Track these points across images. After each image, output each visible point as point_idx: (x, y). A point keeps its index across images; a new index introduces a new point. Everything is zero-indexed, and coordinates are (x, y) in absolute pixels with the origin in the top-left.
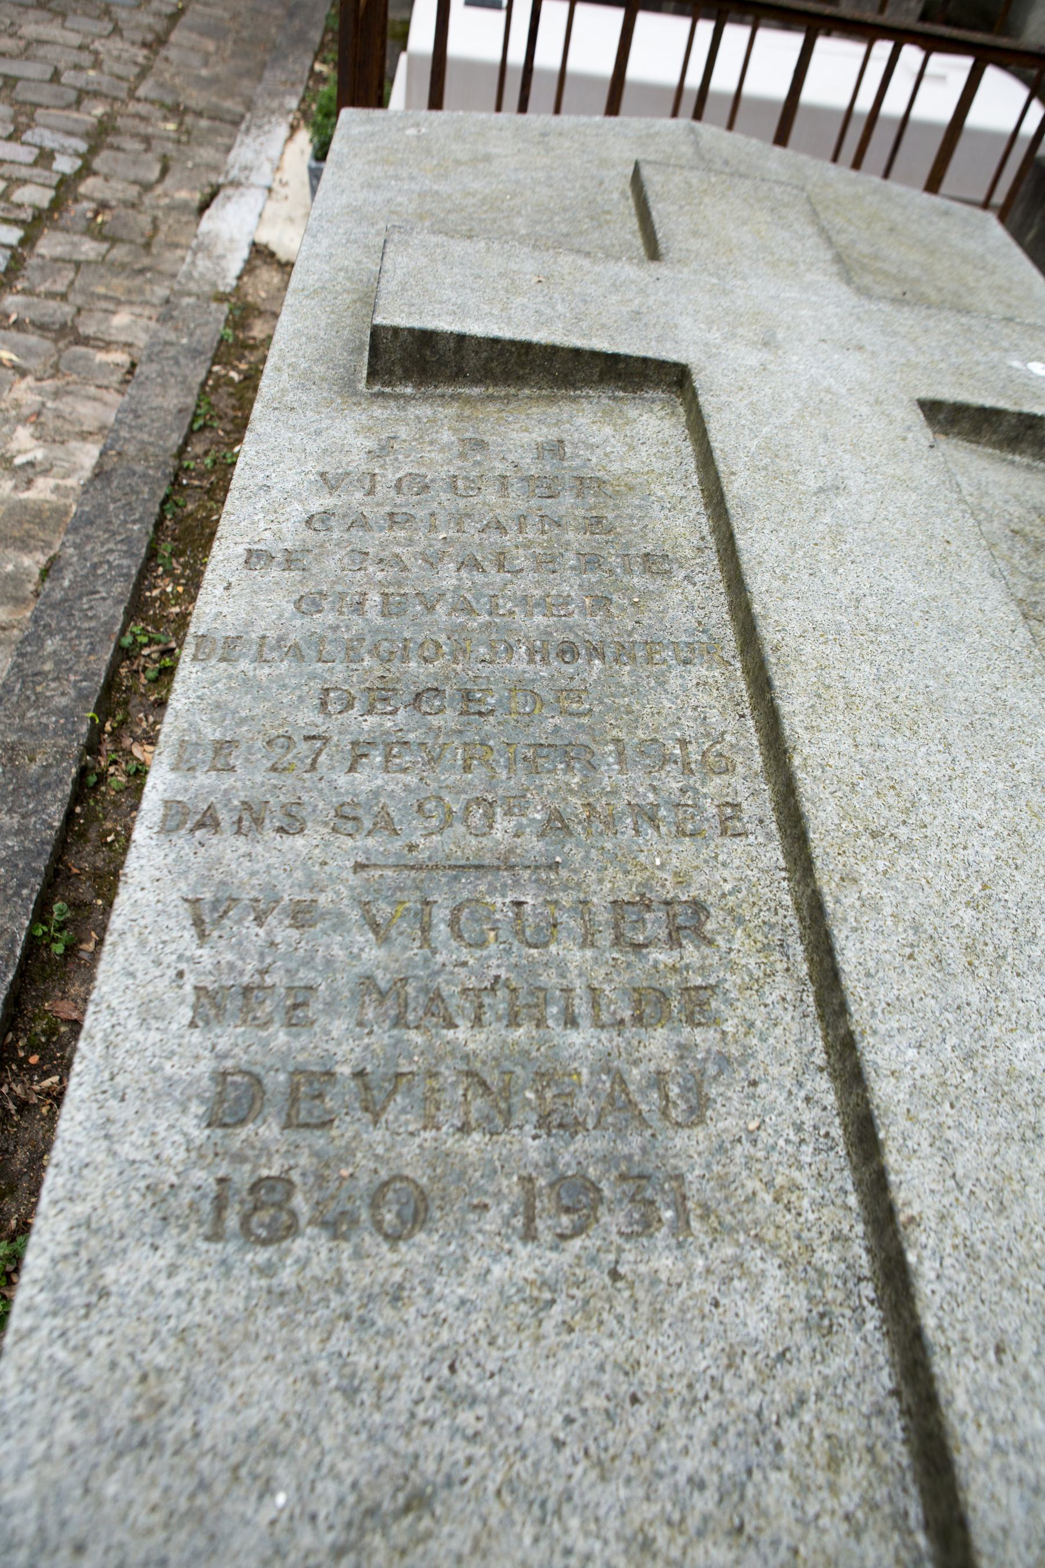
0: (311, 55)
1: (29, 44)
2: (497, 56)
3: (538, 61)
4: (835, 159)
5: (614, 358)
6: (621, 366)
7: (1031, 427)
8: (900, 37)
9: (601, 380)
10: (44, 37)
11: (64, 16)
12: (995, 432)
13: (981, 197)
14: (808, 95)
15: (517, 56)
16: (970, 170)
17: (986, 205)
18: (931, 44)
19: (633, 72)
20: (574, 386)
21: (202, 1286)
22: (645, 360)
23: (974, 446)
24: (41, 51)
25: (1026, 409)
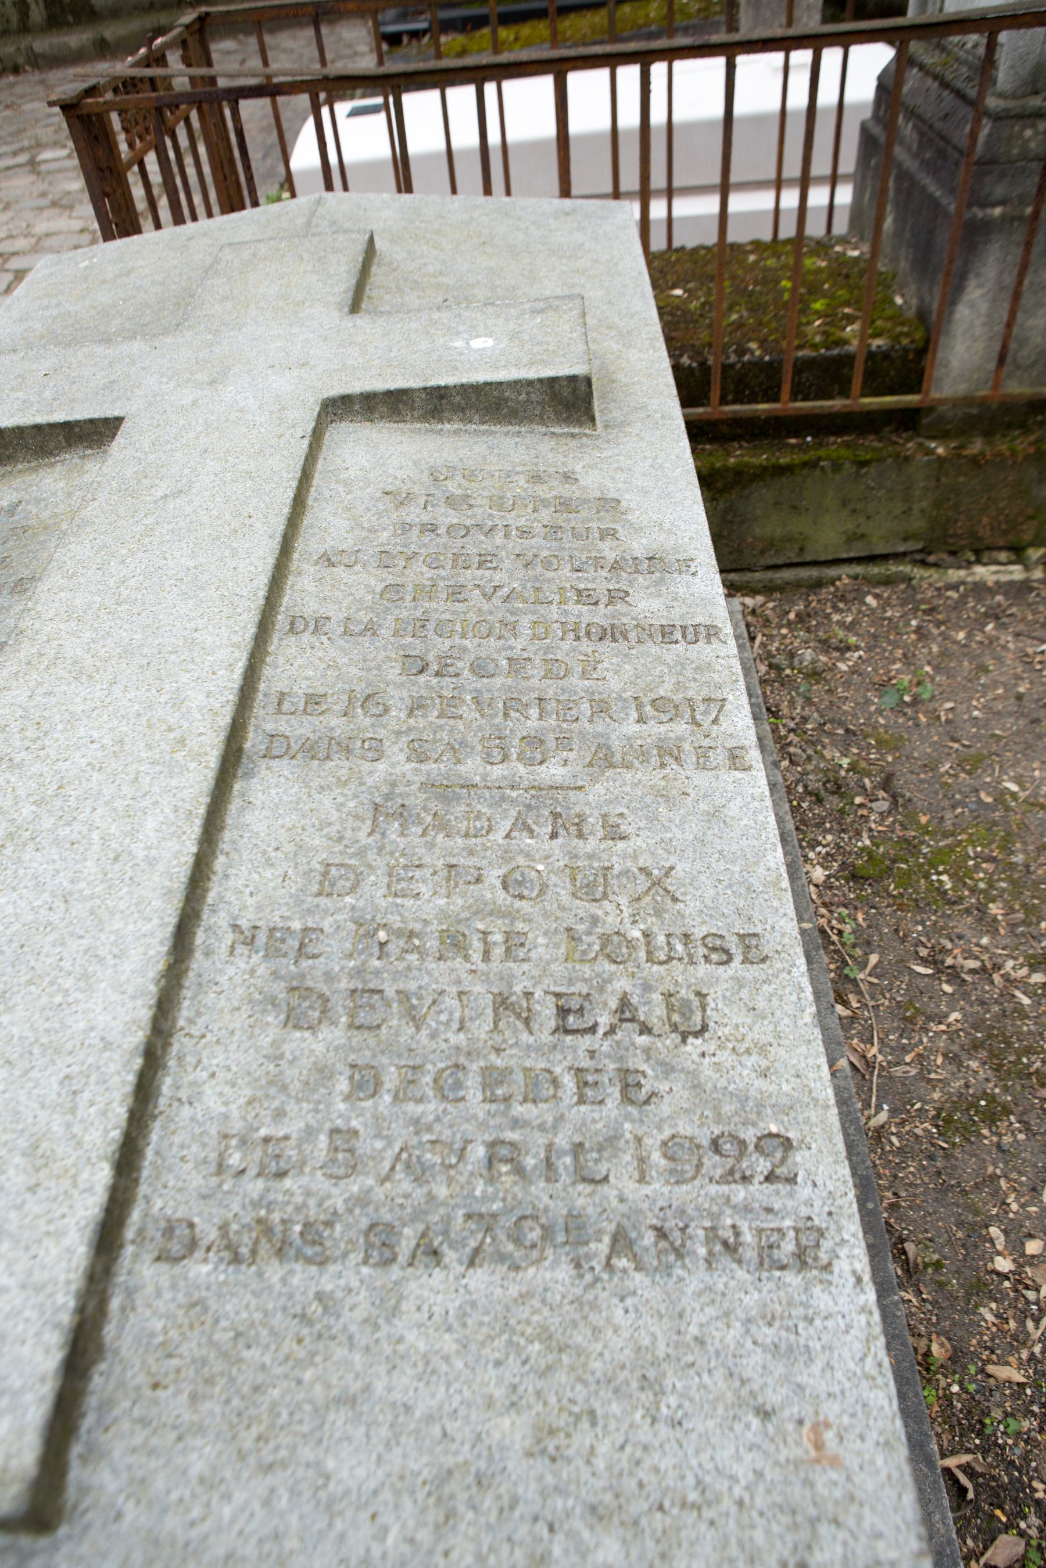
0: (277, 186)
1: (40, 239)
2: (607, 124)
3: (621, 123)
4: (488, 191)
5: (67, 426)
6: (685, 360)
7: (442, 397)
8: (816, 42)
9: (69, 445)
10: (53, 230)
11: (71, 207)
12: (413, 409)
13: (609, 188)
14: (575, 127)
15: (798, 99)
16: (590, 171)
17: (616, 195)
18: (845, 40)
19: (740, 108)
20: (51, 454)
21: (591, 1379)
22: (91, 421)
23: (401, 425)
24: (47, 243)
25: (432, 383)
